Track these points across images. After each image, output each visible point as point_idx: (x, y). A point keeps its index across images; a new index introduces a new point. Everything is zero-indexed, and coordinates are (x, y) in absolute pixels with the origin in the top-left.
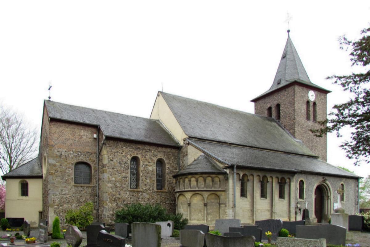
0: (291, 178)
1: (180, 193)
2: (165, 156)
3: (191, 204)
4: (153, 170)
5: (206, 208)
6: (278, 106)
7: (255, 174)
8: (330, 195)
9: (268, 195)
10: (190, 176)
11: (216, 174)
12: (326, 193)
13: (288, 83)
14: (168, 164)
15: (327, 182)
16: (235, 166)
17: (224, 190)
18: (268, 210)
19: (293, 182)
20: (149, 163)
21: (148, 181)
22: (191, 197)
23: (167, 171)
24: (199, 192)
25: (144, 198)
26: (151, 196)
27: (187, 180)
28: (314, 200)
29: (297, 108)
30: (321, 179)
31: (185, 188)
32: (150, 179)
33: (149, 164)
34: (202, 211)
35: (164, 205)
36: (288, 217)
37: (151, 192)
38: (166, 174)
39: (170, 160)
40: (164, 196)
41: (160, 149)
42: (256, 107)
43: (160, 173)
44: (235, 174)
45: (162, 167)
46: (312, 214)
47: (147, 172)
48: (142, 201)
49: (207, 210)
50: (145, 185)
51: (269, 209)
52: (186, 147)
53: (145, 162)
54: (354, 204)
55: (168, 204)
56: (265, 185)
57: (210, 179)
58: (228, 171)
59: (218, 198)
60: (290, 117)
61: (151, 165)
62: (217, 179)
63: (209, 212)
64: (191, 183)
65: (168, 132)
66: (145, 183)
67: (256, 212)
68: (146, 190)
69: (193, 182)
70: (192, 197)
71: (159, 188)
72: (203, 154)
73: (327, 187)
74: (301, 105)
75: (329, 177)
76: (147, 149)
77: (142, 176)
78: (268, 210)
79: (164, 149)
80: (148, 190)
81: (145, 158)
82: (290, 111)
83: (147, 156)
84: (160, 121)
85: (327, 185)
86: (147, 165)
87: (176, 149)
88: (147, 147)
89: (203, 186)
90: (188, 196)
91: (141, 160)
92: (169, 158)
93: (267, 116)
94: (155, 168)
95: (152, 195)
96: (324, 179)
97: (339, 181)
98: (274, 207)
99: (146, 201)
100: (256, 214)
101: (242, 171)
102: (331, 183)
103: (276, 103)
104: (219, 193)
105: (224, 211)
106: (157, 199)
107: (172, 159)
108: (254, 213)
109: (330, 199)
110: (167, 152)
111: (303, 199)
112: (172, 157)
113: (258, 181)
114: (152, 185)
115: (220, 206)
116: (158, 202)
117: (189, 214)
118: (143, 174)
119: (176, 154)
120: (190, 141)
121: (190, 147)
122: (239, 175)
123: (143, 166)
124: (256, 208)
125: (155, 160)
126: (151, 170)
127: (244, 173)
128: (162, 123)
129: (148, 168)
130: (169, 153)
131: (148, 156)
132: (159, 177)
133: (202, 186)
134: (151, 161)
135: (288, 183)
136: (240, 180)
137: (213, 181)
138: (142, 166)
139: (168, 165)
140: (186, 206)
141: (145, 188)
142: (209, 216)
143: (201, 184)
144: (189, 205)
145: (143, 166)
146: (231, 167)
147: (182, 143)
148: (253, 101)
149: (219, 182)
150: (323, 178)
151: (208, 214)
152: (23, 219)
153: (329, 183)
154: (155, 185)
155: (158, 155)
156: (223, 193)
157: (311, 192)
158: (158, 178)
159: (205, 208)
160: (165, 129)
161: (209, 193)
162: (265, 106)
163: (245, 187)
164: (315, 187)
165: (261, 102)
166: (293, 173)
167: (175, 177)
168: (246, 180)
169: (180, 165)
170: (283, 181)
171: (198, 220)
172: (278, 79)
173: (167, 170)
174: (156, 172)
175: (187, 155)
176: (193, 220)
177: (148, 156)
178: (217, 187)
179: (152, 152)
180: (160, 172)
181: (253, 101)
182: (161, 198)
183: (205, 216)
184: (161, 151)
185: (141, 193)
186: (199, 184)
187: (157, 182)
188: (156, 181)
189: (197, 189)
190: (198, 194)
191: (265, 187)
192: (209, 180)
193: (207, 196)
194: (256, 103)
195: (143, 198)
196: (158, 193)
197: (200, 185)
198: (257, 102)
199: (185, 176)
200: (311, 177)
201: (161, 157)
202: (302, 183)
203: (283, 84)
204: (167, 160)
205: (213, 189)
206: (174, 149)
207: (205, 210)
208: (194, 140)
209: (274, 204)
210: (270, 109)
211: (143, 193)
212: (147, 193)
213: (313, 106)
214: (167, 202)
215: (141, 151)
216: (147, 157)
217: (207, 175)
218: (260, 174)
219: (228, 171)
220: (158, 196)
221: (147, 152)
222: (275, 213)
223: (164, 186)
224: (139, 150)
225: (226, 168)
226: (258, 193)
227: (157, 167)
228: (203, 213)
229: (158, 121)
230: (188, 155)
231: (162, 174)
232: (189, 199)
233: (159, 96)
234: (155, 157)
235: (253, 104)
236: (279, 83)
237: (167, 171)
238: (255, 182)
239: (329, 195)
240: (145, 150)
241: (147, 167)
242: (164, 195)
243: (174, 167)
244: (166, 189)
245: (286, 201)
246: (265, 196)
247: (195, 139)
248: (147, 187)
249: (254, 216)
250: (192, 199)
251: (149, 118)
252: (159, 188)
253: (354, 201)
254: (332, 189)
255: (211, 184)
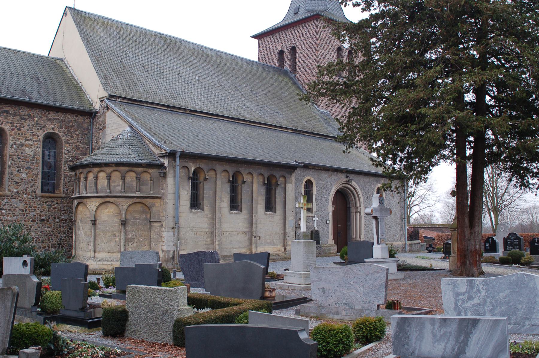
0: (287, 176)
1: (79, 201)
2: (61, 128)
3: (98, 222)
4: (35, 154)
5: (125, 228)
6: (293, 50)
7: (219, 168)
8: (360, 206)
9: (245, 206)
10: (96, 169)
11: (144, 167)
12: (354, 202)
13: (308, 15)
14: (68, 143)
15: (353, 183)
16: (178, 154)
17: (160, 196)
18: (245, 233)
19: (291, 183)
20: (28, 140)
21: (24, 175)
22: (98, 207)
23: (65, 157)
24: (112, 200)
25: (12, 209)
26: (28, 206)
27: (91, 176)
28: (331, 213)
29: (321, 57)
30: (343, 178)
31: (88, 191)
32: (27, 172)
33: (27, 142)
34: (118, 234)
35: (57, 222)
36: (282, 245)
37: (30, 196)
38: (63, 163)
39: (72, 137)
40: (56, 205)
41: (52, 115)
42: (260, 48)
43: (52, 161)
44: (177, 168)
45: (55, 149)
46: (328, 238)
47: (23, 158)
48: (8, 216)
49: (125, 234)
50: (17, 183)
51: (247, 230)
52: (104, 113)
53: (19, 139)
54: (399, 221)
55: (66, 220)
56: (239, 187)
57: (133, 175)
58: (166, 162)
59: (147, 210)
60: (311, 70)
61: (32, 145)
62: (146, 177)
63: (129, 236)
64: (98, 182)
65: (77, 82)
66: (16, 179)
67: (220, 235)
68: (18, 192)
69: (103, 181)
70: (100, 209)
71: (48, 190)
72: (129, 129)
73: (354, 192)
74: (328, 52)
75: (356, 176)
76: (23, 113)
77: (10, 167)
78: (245, 233)
79: (61, 116)
80: (23, 193)
81: (18, 132)
82: (311, 61)
83: (23, 127)
84: (65, 61)
85: (354, 189)
86: (22, 145)
87: (85, 116)
88: (25, 111)
89: (119, 188)
90: (92, 207)
91: (11, 135)
92: (70, 133)
93: (276, 66)
94: (39, 150)
95: (32, 204)
96: (349, 178)
97: (375, 183)
98: (254, 226)
99: (18, 216)
100: (220, 240)
101: (193, 163)
102: (361, 185)
103: (290, 44)
104: (148, 202)
105: (159, 235)
106: (41, 212)
107: (77, 135)
108: (217, 237)
109: (360, 213)
110: (66, 120)
111: (312, 213)
112: (76, 131)
113: (225, 180)
114: (32, 184)
115: (150, 224)
116: (43, 218)
117: (92, 241)
118: (13, 162)
119: (85, 126)
120: (111, 105)
121: (109, 113)
122: (187, 170)
123: (14, 146)
124: (220, 229)
125: (41, 135)
126: (30, 155)
127: (198, 166)
128: (68, 66)
129: (24, 150)
130: (71, 124)
131: (27, 127)
132: (50, 167)
133: (118, 188)
134: (31, 137)
135: (283, 185)
136: (190, 178)
137: (138, 179)
138: (12, 145)
139: (68, 145)
140: (89, 225)
141: (15, 190)
142: (130, 244)
143: (116, 184)
144: (122, 224)
145: (14, 146)
146: (171, 155)
147: (97, 106)
148: (255, 37)
149: (150, 182)
150: (347, 177)
151: (126, 240)
152: (504, 238)
153: (356, 184)
154: (39, 184)
155: (48, 127)
156: (157, 202)
157: (327, 200)
158: (46, 169)
159: (123, 229)
160: (73, 76)
161: (129, 201)
162: (274, 47)
163: (201, 192)
164: (333, 192)
165: (268, 40)
166: (290, 168)
167: (73, 168)
168: (202, 178)
169: (93, 147)
170: (274, 181)
171: (109, 252)
172: (296, 5)
173: (66, 154)
174: (43, 158)
175: (104, 128)
176: (99, 252)
177: (27, 127)
178: (147, 191)
179: (34, 120)
180: (52, 158)
181: (255, 37)
182: (51, 208)
183: (122, 244)
184: (54, 119)
185: (6, 200)
186: (112, 184)
187: (43, 178)
188: (40, 176)
189: (108, 194)
190: (110, 202)
191: (239, 191)
192: (131, 177)
193: (125, 207)
194: (260, 42)
195: (9, 210)
196: (43, 200)
197: (115, 186)
198: (262, 39)
199: (88, 169)
200: (324, 175)
201: (53, 129)
202: (309, 184)
203: (302, 14)
204: (66, 135)
205: (138, 194)
206: (81, 116)
207: (123, 233)
208: (120, 102)
209: (254, 221)
210: (281, 53)
211: (12, 198)
212: (20, 200)
213: (347, 56)
214: (63, 217)
215: (10, 118)
216: (23, 129)
217: (127, 169)
218: (228, 168)
219: (166, 162)
220: (45, 205)
221: (25, 119)
222: (258, 238)
223: (59, 186)
224: (7, 116)
225: (163, 156)
226: (224, 203)
227: (43, 148)
228: (118, 239)
229: (62, 60)
230: (106, 129)
231: (55, 162)
232: (94, 213)
233: (66, 14)
234: (41, 129)
235: (256, 41)
236: (296, 13)
237: (66, 157)
238: (219, 183)
239: (358, 205)
240: (20, 115)
241: (23, 148)
242: (57, 203)
243: (81, 149)
244: (62, 191)
245: (278, 216)
246: (239, 208)
247: (122, 101)
248: (20, 189)
249: (217, 243)
250: (99, 212)
251: (45, 54)
252: (48, 190)
253: (399, 216)
254: (363, 196)
255: (135, 184)
